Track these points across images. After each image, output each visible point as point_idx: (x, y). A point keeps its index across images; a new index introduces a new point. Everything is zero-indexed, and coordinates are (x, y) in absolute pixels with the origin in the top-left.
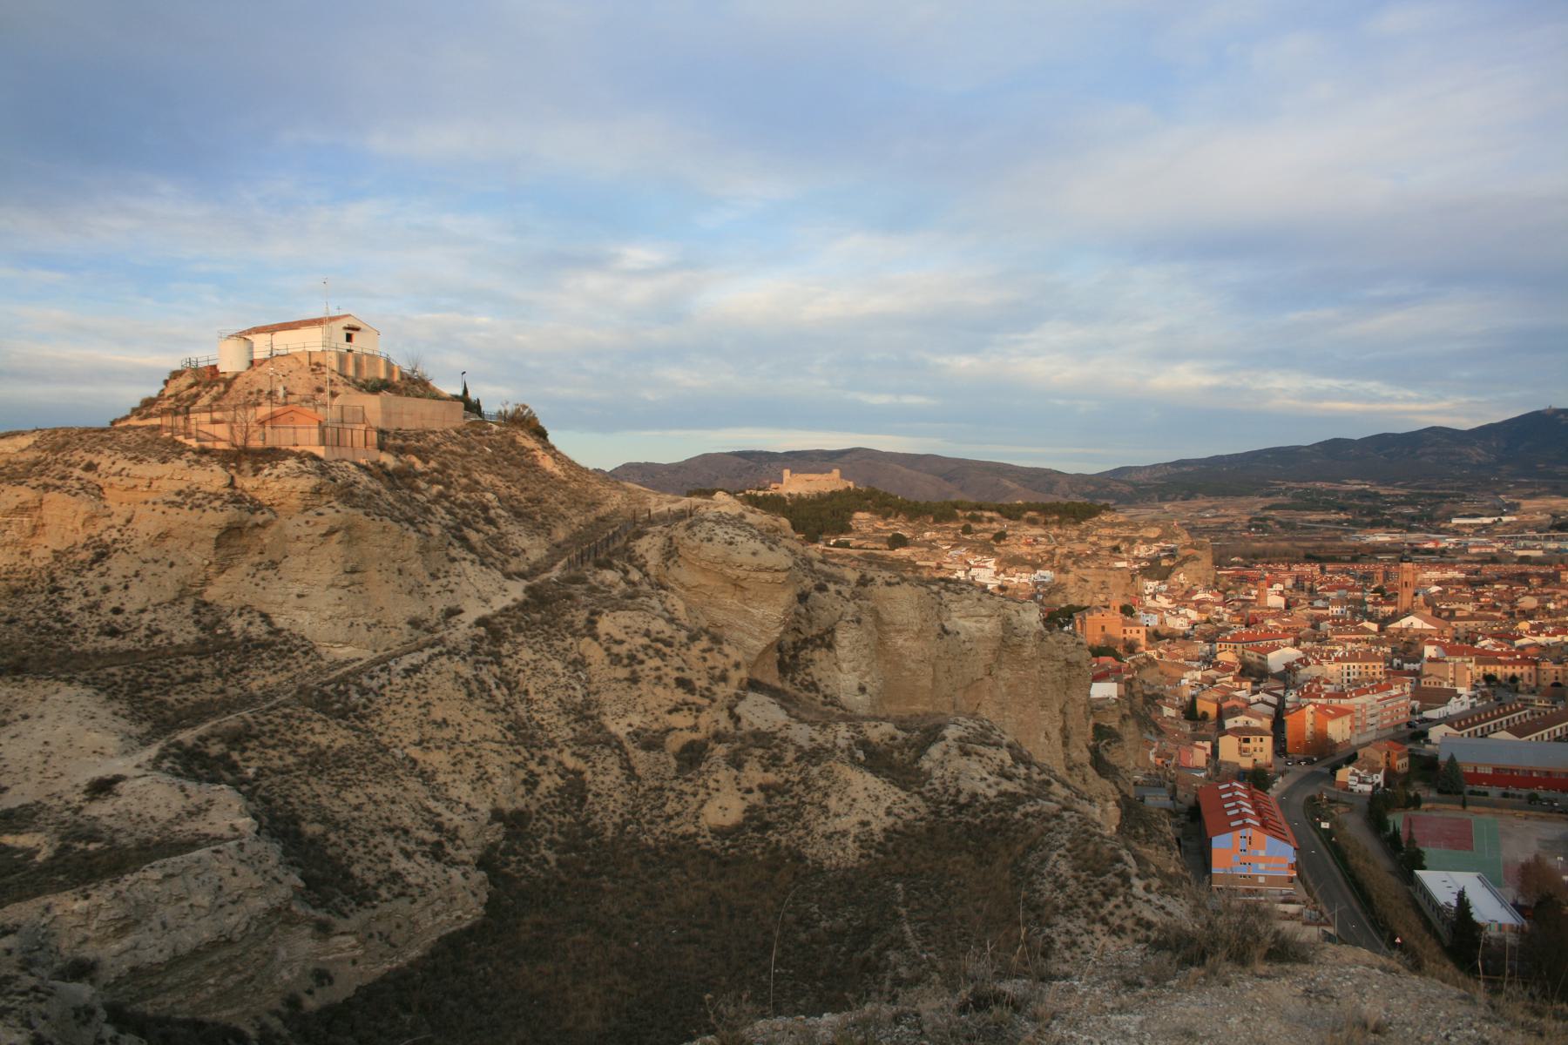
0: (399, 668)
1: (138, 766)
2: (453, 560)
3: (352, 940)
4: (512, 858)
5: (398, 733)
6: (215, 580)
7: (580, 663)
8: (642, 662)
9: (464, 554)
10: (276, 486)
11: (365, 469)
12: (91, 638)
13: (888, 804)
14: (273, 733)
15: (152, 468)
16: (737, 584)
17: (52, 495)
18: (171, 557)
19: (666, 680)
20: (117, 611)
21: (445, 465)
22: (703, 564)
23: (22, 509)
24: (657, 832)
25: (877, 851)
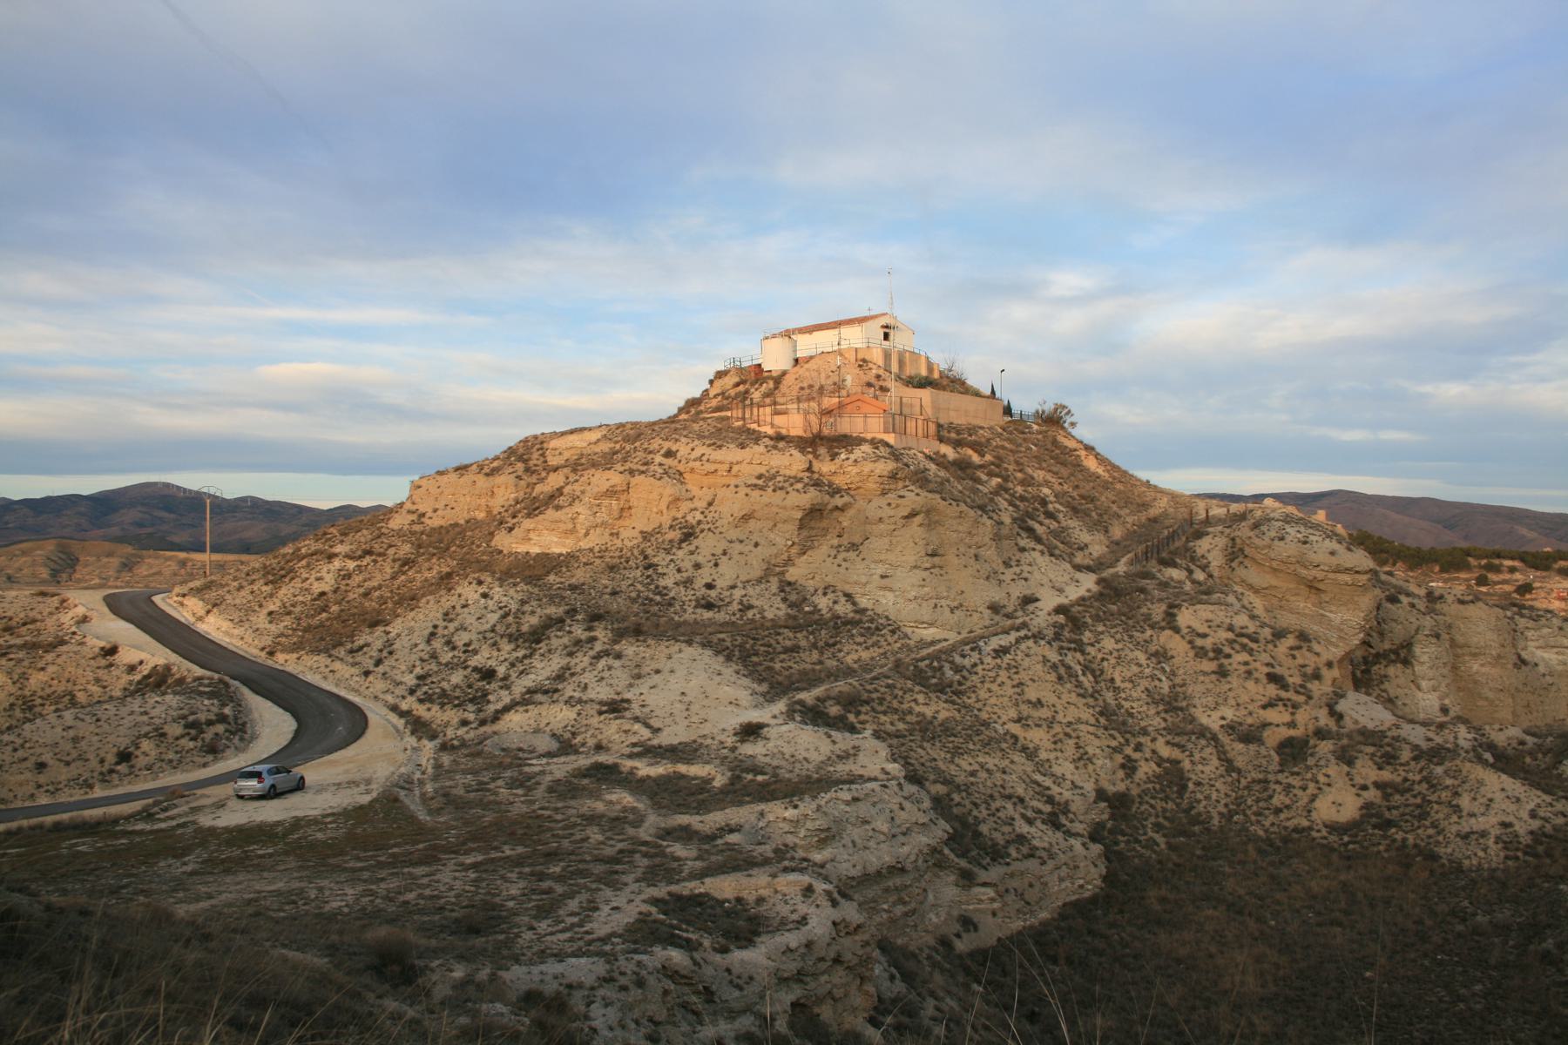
0: (989, 649)
1: (775, 717)
2: (1023, 550)
3: (991, 892)
4: (1121, 838)
5: (996, 709)
6: (797, 561)
7: (1161, 656)
8: (1228, 656)
9: (1032, 544)
10: (854, 470)
11: (929, 458)
12: (690, 610)
13: (1532, 806)
14: (881, 700)
15: (731, 453)
16: (1313, 587)
17: (639, 479)
18: (755, 538)
19: (1256, 675)
20: (710, 586)
21: (998, 458)
22: (1274, 564)
23: (611, 493)
24: (1267, 823)
25: (1526, 853)
